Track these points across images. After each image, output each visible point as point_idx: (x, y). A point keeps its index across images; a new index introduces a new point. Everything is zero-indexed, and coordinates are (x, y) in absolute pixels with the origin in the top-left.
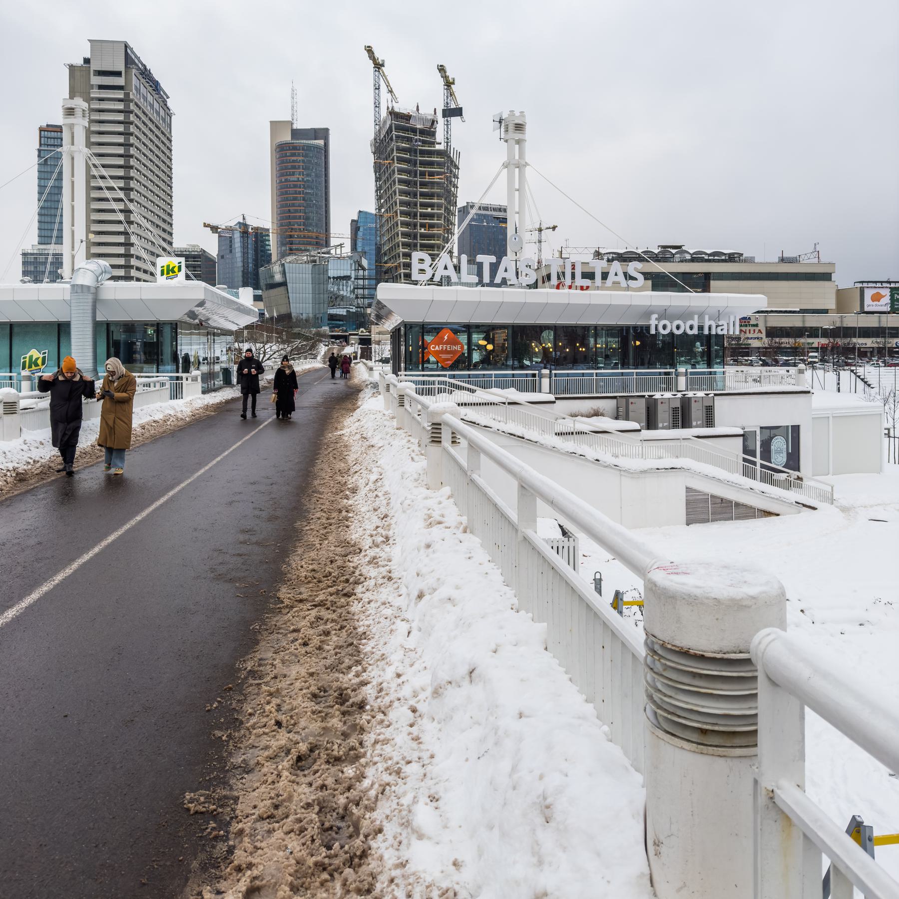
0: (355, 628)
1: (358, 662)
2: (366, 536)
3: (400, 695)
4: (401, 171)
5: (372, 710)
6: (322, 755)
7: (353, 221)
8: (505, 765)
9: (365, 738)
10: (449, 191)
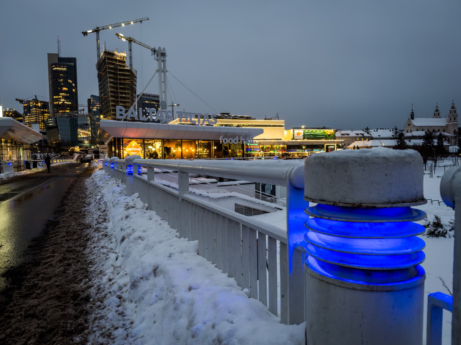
0: (86, 261)
1: (86, 277)
2: (94, 221)
3: (111, 290)
4: (110, 78)
5: (94, 301)
6: (59, 331)
7: (89, 99)
8: (184, 322)
9: (89, 317)
10: (133, 88)
